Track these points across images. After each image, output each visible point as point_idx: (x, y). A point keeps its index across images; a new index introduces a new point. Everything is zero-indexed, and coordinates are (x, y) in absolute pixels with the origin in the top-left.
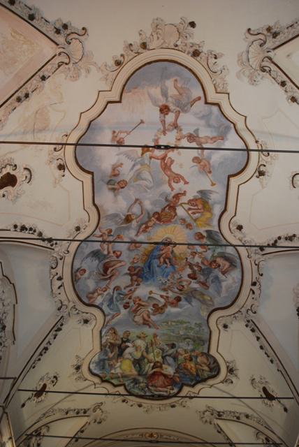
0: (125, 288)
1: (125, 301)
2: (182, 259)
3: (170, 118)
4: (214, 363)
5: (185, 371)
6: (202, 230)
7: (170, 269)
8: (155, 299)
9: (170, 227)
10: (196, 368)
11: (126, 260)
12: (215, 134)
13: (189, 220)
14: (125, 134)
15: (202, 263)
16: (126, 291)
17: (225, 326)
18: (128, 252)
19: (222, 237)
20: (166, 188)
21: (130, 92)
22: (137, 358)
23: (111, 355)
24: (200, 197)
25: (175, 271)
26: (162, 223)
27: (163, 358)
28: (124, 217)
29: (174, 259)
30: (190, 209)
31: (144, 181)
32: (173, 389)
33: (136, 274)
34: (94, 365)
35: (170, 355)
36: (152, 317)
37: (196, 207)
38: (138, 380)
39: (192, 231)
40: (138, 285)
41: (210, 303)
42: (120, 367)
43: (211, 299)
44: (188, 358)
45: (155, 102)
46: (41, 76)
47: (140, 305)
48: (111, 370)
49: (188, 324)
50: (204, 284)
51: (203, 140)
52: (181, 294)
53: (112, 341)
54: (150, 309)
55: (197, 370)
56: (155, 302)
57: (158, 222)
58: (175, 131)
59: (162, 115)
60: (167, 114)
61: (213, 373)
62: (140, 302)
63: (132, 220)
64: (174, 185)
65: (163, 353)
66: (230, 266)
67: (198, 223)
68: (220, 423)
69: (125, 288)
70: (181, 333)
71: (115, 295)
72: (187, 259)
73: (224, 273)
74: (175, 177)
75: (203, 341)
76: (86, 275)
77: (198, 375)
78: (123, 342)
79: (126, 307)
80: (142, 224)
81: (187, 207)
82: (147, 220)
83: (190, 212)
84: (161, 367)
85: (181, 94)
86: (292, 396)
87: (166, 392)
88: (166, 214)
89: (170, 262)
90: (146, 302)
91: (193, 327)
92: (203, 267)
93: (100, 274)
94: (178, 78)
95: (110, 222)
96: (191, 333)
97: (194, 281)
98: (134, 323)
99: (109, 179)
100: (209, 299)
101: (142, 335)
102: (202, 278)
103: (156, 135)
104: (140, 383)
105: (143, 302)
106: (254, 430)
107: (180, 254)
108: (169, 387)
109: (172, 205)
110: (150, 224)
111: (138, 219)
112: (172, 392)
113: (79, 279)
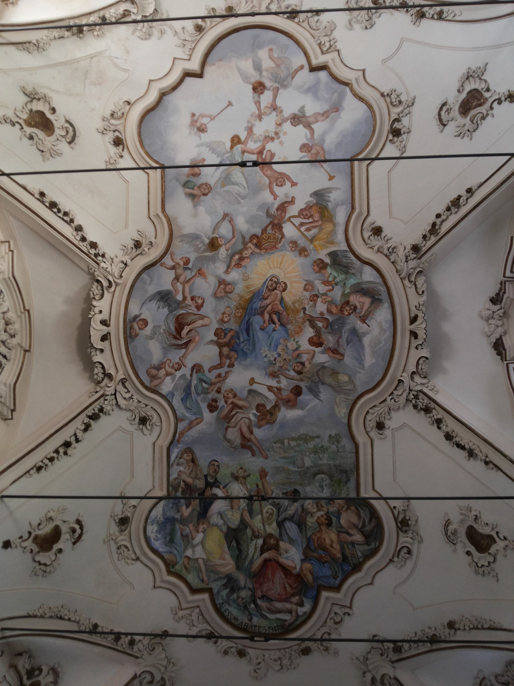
0: (210, 371)
1: (210, 396)
2: (298, 311)
3: (266, 98)
4: (370, 521)
5: (321, 552)
6: (323, 255)
7: (280, 330)
8: (260, 394)
9: (276, 256)
10: (340, 542)
11: (211, 315)
12: (326, 107)
13: (302, 242)
14: (209, 119)
15: (329, 311)
16: (212, 376)
17: (380, 426)
18: (214, 300)
19: (353, 257)
20: (267, 196)
21: (214, 64)
22: (233, 526)
23: (186, 512)
24: (315, 201)
25: (288, 335)
26: (263, 252)
27: (280, 524)
28: (207, 241)
29: (285, 313)
30: (302, 224)
31: (236, 187)
32: (301, 604)
33: (226, 344)
34: (155, 528)
35: (290, 519)
36: (256, 430)
37: (311, 220)
38: (236, 581)
39: (308, 259)
40: (231, 365)
41: (350, 387)
42: (202, 543)
43: (350, 378)
44: (323, 519)
45: (245, 78)
46: (101, 16)
47: (235, 406)
48: (186, 548)
49: (317, 440)
50: (335, 351)
51: (312, 120)
52: (302, 380)
53: (189, 480)
54: (252, 415)
55: (342, 548)
56: (259, 400)
57: (257, 250)
58: (274, 113)
59: (256, 95)
60: (262, 93)
61: (373, 546)
62: (236, 401)
63: (221, 246)
64: (276, 189)
65: (278, 515)
66: (372, 303)
67: (316, 243)
69: (210, 371)
70: (308, 462)
71: (194, 382)
72: (304, 309)
73: (363, 319)
74: (278, 178)
75: (345, 472)
76: (148, 330)
77: (345, 558)
78: (209, 485)
79: (212, 407)
80: (234, 254)
81: (297, 221)
82: (240, 246)
83: (303, 229)
84: (276, 547)
85: (278, 66)
87: (290, 612)
88: (269, 238)
89: (279, 321)
90: (245, 399)
91: (326, 444)
92: (331, 318)
93: (171, 334)
94: (274, 47)
95: (187, 246)
96: (325, 460)
97: (320, 349)
98: (226, 443)
99: (187, 179)
100: (346, 379)
101: (241, 473)
102: (330, 340)
103: (249, 122)
104: (239, 589)
105: (240, 399)
107: (294, 303)
108: (295, 599)
109: (276, 222)
110: (246, 253)
111: (228, 246)
112: (301, 610)
113: (137, 335)
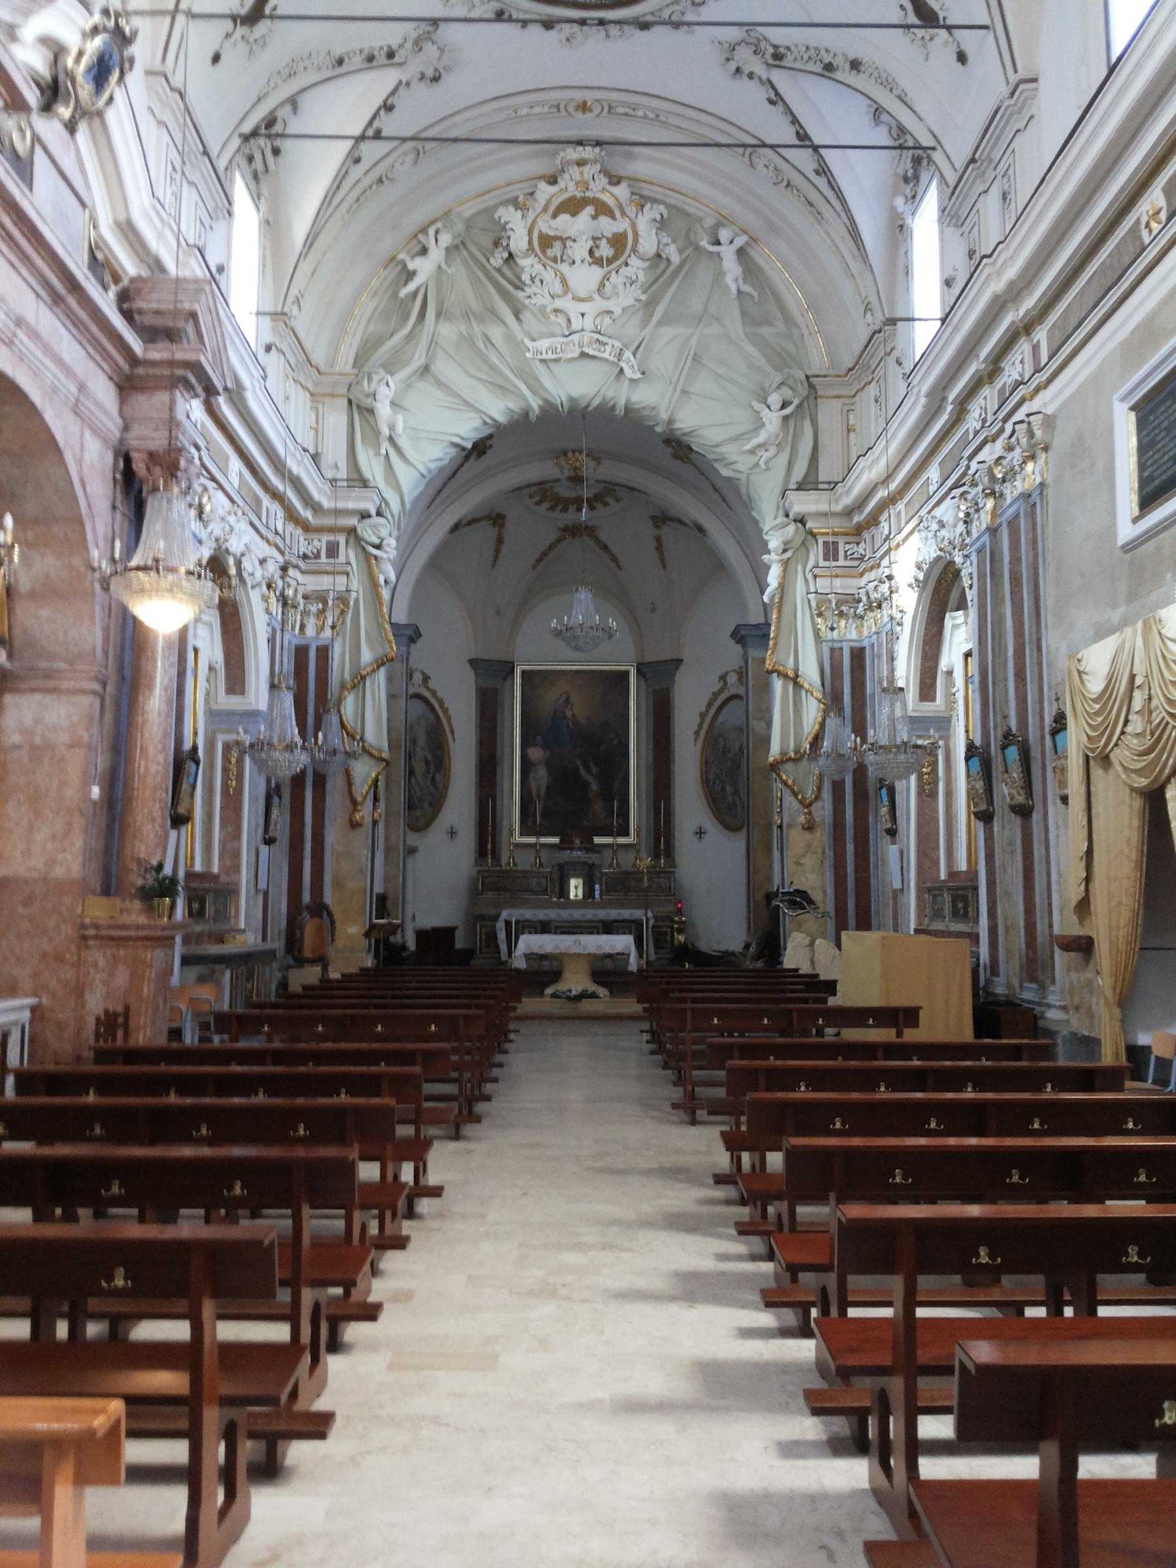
68: (778, 77)
86: (985, 21)
106: (868, 102)
